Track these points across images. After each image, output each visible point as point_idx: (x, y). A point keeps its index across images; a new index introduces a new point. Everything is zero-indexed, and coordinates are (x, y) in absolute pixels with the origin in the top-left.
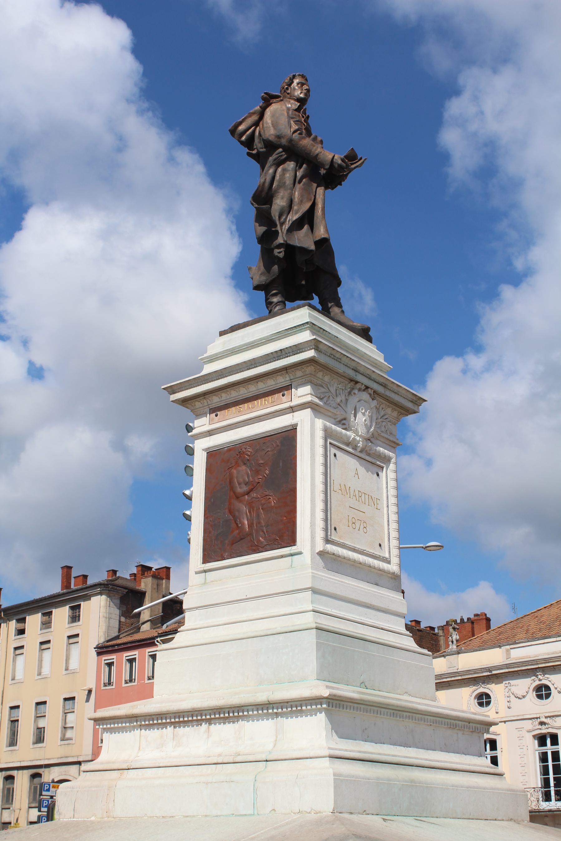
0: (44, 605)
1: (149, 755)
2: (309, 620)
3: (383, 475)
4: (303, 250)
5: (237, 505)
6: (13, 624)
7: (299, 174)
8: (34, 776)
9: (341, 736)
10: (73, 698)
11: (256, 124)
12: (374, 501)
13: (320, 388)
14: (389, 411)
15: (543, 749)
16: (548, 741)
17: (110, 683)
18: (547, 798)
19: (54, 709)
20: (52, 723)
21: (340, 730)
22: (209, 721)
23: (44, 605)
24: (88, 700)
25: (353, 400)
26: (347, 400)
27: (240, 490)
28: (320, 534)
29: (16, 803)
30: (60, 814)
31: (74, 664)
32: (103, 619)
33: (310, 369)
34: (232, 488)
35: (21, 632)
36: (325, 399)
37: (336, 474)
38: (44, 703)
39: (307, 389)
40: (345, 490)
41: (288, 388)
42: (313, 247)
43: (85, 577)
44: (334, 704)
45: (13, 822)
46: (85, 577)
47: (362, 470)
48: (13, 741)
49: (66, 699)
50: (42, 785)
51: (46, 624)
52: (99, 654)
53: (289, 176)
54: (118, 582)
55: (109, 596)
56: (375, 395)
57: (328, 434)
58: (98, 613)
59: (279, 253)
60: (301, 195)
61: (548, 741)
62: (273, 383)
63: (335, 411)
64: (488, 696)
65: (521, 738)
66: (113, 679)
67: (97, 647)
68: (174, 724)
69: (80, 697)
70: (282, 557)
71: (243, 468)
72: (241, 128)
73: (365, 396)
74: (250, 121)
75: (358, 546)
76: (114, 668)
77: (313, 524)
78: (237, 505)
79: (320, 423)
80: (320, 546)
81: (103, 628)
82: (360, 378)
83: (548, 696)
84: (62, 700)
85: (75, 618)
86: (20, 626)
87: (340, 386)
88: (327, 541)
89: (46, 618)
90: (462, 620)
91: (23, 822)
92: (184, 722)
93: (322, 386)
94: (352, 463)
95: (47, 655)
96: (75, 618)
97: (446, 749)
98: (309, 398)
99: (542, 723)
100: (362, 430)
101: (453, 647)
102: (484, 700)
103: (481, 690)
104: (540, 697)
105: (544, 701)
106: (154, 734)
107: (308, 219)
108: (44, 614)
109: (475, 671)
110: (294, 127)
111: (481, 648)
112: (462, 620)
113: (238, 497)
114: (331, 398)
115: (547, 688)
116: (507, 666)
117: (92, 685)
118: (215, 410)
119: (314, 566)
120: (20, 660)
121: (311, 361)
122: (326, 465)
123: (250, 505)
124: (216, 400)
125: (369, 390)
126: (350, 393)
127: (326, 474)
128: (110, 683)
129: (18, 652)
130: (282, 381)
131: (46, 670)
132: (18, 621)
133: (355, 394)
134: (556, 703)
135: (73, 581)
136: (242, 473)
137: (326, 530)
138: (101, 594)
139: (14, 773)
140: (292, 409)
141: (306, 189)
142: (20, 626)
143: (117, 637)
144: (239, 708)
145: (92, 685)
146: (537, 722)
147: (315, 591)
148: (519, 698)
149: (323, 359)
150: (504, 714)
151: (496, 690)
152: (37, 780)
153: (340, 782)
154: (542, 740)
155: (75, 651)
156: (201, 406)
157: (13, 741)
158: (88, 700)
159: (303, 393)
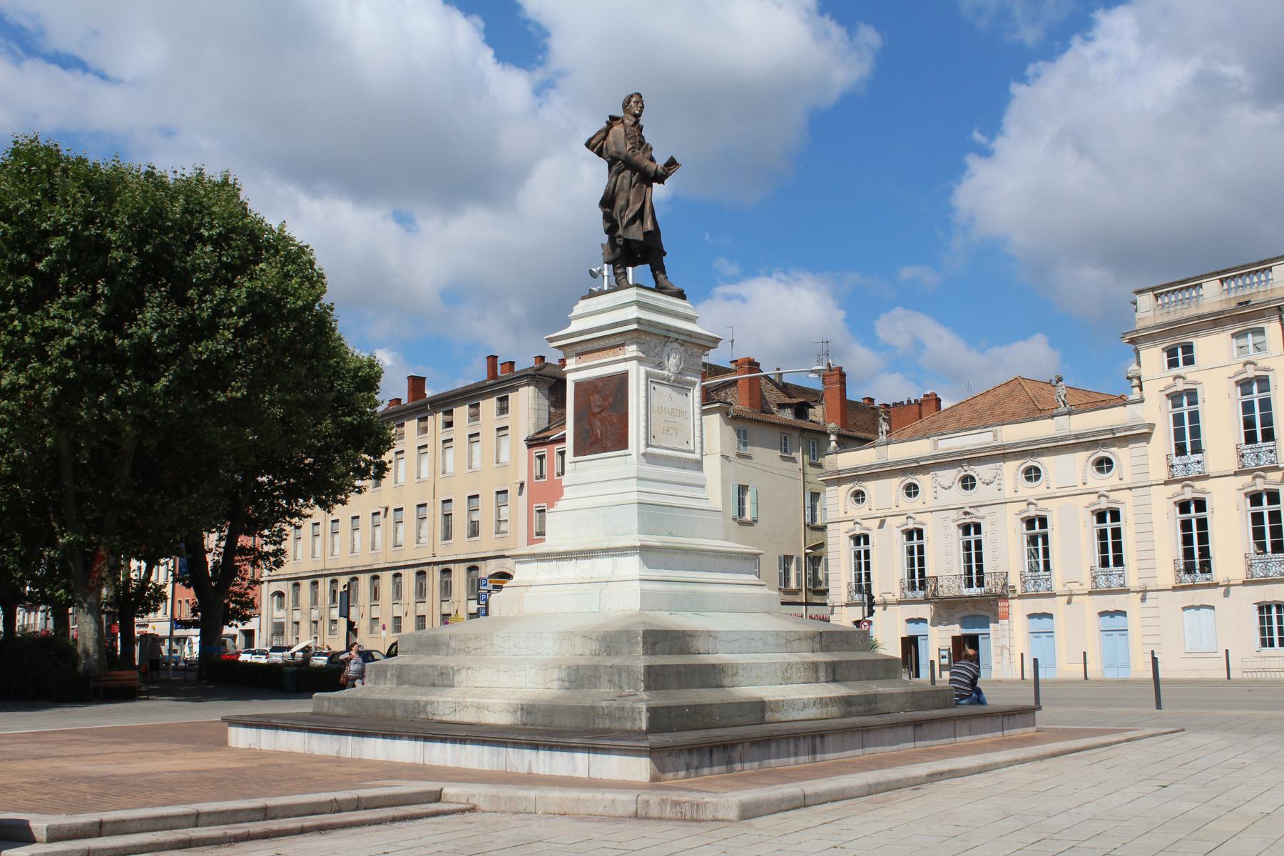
0: (471, 396)
1: (542, 578)
2: (634, 497)
3: (690, 394)
4: (636, 241)
5: (593, 420)
6: (440, 417)
7: (634, 179)
8: (471, 569)
9: (650, 567)
10: (506, 492)
11: (604, 139)
12: (683, 414)
16: (972, 530)
17: (542, 476)
18: (970, 585)
19: (487, 502)
20: (486, 517)
21: (648, 564)
22: (576, 558)
23: (471, 396)
24: (520, 494)
25: (667, 350)
27: (596, 410)
28: (643, 442)
29: (455, 597)
31: (504, 457)
32: (531, 411)
33: (635, 335)
34: (590, 409)
35: (449, 424)
37: (655, 401)
38: (477, 496)
39: (634, 347)
40: (661, 410)
41: (623, 345)
42: (642, 239)
43: (512, 363)
44: (644, 551)
45: (453, 613)
46: (512, 363)
47: (674, 394)
48: (447, 535)
49: (498, 493)
50: (479, 580)
51: (474, 417)
52: (529, 446)
53: (626, 182)
54: (547, 371)
55: (536, 386)
56: (683, 343)
57: (648, 375)
58: (526, 401)
59: (619, 241)
60: (635, 198)
61: (972, 530)
64: (916, 487)
65: (946, 527)
66: (545, 472)
67: (527, 440)
68: (557, 560)
69: (513, 490)
71: (597, 396)
72: (594, 142)
73: (676, 345)
74: (599, 137)
75: (670, 446)
76: (545, 461)
77: (638, 437)
78: (593, 420)
79: (643, 369)
80: (642, 451)
81: (533, 420)
82: (671, 334)
83: (973, 486)
84: (494, 494)
85: (503, 410)
86: (448, 418)
88: (648, 445)
89: (473, 410)
90: (909, 401)
91: (463, 614)
94: (667, 390)
95: (476, 447)
96: (503, 410)
97: (725, 571)
98: (635, 354)
99: (966, 513)
100: (673, 369)
101: (883, 438)
102: (912, 490)
103: (910, 480)
104: (965, 487)
105: (969, 492)
106: (545, 565)
107: (640, 215)
108: (471, 406)
109: (903, 462)
110: (629, 146)
111: (911, 439)
112: (909, 401)
113: (594, 415)
115: (972, 479)
116: (934, 457)
117: (524, 478)
118: (579, 355)
119: (639, 462)
120: (450, 453)
121: (636, 330)
122: (647, 397)
123: (601, 421)
124: (579, 349)
127: (647, 403)
128: (542, 476)
129: (447, 445)
131: (476, 463)
132: (446, 413)
134: (981, 493)
135: (499, 367)
136: (596, 399)
137: (647, 439)
138: (528, 385)
139: (451, 566)
140: (626, 360)
141: (639, 192)
142: (448, 418)
143: (547, 429)
144: (593, 551)
145: (524, 478)
146: (961, 512)
147: (639, 479)
150: (931, 504)
151: (923, 480)
152: (473, 573)
153: (644, 594)
154: (966, 529)
155: (505, 443)
157: (447, 535)
158: (520, 494)
159: (632, 350)
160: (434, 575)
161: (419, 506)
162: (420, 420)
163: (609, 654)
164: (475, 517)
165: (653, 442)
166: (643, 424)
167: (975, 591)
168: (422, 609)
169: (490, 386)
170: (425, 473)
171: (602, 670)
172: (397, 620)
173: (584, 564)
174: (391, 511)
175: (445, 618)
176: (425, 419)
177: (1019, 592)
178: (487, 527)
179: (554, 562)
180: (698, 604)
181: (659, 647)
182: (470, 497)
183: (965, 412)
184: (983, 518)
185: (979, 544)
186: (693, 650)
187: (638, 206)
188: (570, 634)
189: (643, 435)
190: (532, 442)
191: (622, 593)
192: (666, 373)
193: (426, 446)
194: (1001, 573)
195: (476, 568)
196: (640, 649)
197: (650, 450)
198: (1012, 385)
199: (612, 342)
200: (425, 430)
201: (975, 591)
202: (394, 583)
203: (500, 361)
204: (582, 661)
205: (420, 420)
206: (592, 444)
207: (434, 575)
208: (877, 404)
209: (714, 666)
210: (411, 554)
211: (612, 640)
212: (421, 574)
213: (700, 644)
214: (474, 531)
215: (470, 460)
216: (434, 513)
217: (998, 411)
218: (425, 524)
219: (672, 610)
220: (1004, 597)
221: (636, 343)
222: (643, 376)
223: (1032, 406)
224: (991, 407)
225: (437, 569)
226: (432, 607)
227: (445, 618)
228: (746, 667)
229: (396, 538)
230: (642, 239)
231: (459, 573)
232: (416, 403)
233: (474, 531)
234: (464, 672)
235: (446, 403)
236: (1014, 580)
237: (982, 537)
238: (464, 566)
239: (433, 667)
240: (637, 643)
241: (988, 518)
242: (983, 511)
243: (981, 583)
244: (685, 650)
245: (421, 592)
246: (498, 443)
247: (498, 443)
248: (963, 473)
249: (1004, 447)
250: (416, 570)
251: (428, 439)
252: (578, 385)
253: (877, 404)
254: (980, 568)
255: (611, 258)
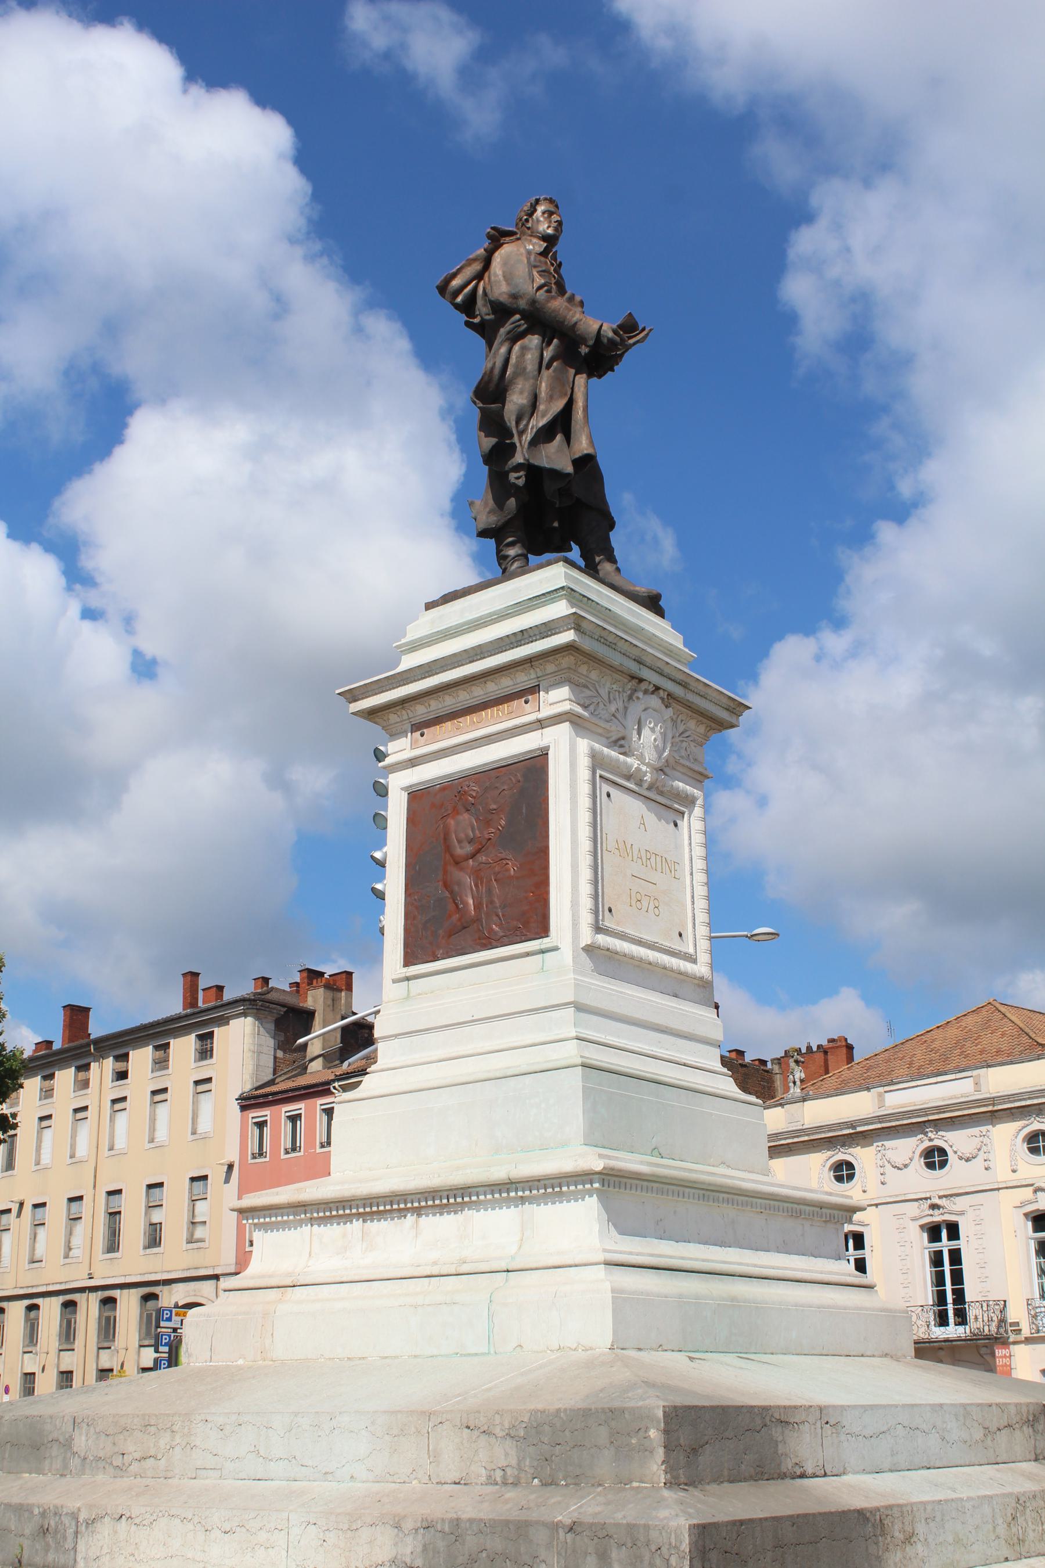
0: (157, 1034)
1: (325, 1265)
2: (571, 1052)
3: (684, 824)
5: (457, 874)
6: (109, 1064)
7: (547, 354)
10: (205, 1178)
11: (479, 277)
12: (670, 866)
13: (585, 690)
14: (692, 724)
15: (936, 1246)
16: (944, 1234)
19: (176, 1194)
20: (172, 1216)
21: (620, 1222)
22: (418, 1211)
23: (157, 1034)
24: (227, 1180)
25: (636, 709)
26: (626, 708)
28: (586, 919)
30: (190, 1356)
31: (205, 1125)
32: (248, 1055)
33: (567, 661)
34: (448, 848)
35: (122, 1075)
36: (592, 708)
37: (610, 824)
38: (160, 1185)
39: (562, 693)
40: (624, 849)
41: (534, 690)
42: (569, 469)
43: (220, 989)
45: (116, 1368)
46: (220, 989)
47: (651, 818)
48: (113, 1245)
49: (193, 1179)
50: (159, 1312)
51: (161, 1063)
52: (244, 1108)
53: (531, 357)
55: (257, 1018)
56: (670, 699)
60: (551, 388)
61: (944, 1234)
62: (510, 683)
63: (607, 726)
64: (850, 1166)
66: (267, 1147)
67: (241, 1098)
68: (364, 1217)
69: (216, 1175)
70: (528, 954)
72: (456, 283)
73: (654, 701)
75: (646, 937)
76: (267, 1131)
77: (575, 904)
78: (457, 874)
79: (584, 745)
80: (587, 936)
81: (250, 1067)
82: (646, 673)
83: (943, 1164)
85: (205, 1053)
86: (121, 1066)
87: (614, 686)
88: (598, 929)
89: (160, 1054)
90: (809, 1048)
91: (131, 1369)
92: (379, 1212)
93: (587, 687)
95: (162, 1110)
96: (205, 1053)
97: (786, 1248)
98: (566, 706)
99: (934, 1207)
100: (650, 755)
101: (796, 1091)
102: (844, 1172)
104: (930, 1166)
105: (937, 1173)
106: (332, 1232)
108: (157, 1048)
109: (830, 1127)
110: (539, 281)
111: (839, 1092)
112: (809, 1048)
113: (457, 862)
114: (601, 705)
115: (942, 1152)
116: (880, 1119)
117: (234, 1157)
118: (419, 727)
120: (121, 1119)
121: (569, 648)
124: (421, 711)
125: (661, 692)
126: (630, 698)
127: (594, 825)
130: (523, 679)
131: (161, 1135)
133: (638, 698)
134: (955, 1175)
135: (201, 994)
136: (464, 824)
137: (596, 912)
138: (245, 1014)
139: (116, 1293)
140: (541, 724)
142: (121, 1066)
143: (271, 1082)
144: (465, 1190)
145: (234, 1157)
146: (926, 1205)
147: (580, 1008)
148: (899, 1169)
149: (587, 645)
151: (862, 1156)
152: (151, 1304)
154: (934, 1232)
155: (207, 1104)
156: (398, 720)
157: (113, 1245)
158: (227, 1180)
159: (557, 699)
160: (89, 1308)
161: (71, 1200)
162: (79, 1069)
163: (549, 1483)
164: (156, 1217)
165: (608, 923)
166: (586, 874)
167: (953, 1331)
168: (68, 1361)
169: (186, 1016)
170: (82, 1151)
171: (541, 1536)
172: (29, 1378)
173: (439, 1227)
174: (28, 1208)
175: (104, 1373)
176: (86, 1067)
177: (1026, 1332)
178: (174, 1234)
179: (357, 1224)
180: (747, 1335)
181: (706, 1458)
182: (150, 1187)
183: (918, 1052)
184: (962, 1213)
185: (956, 1256)
186: (788, 1465)
187: (559, 405)
188: (428, 1419)
189: (586, 903)
190: (248, 1102)
191: (557, 1303)
192: (633, 762)
193: (85, 1108)
194: (996, 1302)
195: (154, 1297)
196: (656, 1468)
197: (602, 939)
198: (984, 1012)
199: (506, 684)
200: (85, 1084)
201: (953, 1331)
202: (27, 1319)
203: (203, 983)
204: (469, 1506)
205: (79, 1069)
206: (451, 933)
207: (89, 1308)
208: (748, 1058)
209: (861, 1515)
210: (57, 1274)
211: (558, 1441)
212: (70, 1306)
213: (803, 1447)
214: (154, 1238)
215: (153, 1129)
216: (94, 1210)
217: (971, 1049)
218: (80, 1228)
219: (692, 1350)
220: (1001, 1340)
221: (569, 681)
222: (584, 763)
223: (1025, 1039)
224: (958, 1044)
225: (95, 1298)
226: (82, 1360)
227: (66, 1377)
228: (935, 1512)
229: (33, 1249)
230: (569, 469)
231: (129, 1305)
232: (72, 1044)
233: (154, 1238)
234: (105, 1528)
235: (119, 1044)
236: (1017, 1313)
237: (962, 1244)
238: (135, 1294)
239: (20, 1510)
240: (647, 1450)
241: (971, 1214)
242: (960, 1203)
243: (962, 1317)
244: (769, 1469)
245: (68, 1333)
246: (195, 1104)
247: (195, 1104)
248: (927, 1144)
249: (993, 1101)
250: (62, 1299)
251: (89, 1098)
252: (416, 796)
253: (748, 1058)
254: (959, 1296)
255: (487, 519)
